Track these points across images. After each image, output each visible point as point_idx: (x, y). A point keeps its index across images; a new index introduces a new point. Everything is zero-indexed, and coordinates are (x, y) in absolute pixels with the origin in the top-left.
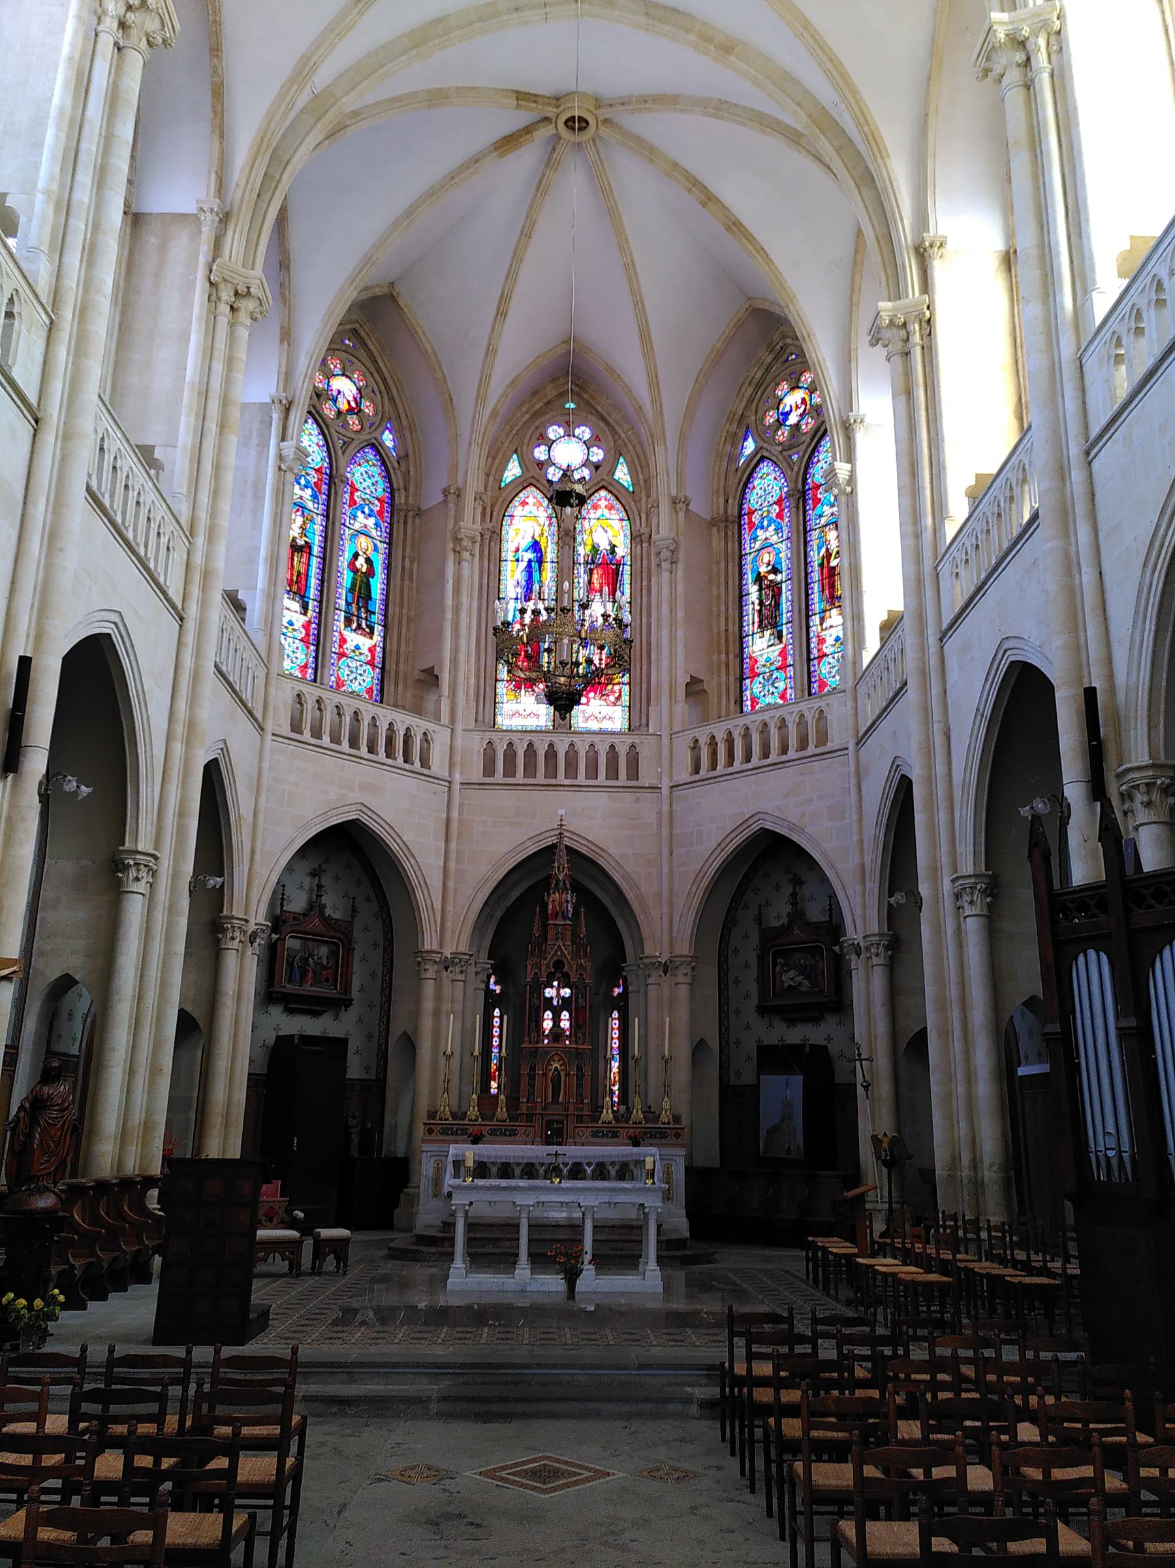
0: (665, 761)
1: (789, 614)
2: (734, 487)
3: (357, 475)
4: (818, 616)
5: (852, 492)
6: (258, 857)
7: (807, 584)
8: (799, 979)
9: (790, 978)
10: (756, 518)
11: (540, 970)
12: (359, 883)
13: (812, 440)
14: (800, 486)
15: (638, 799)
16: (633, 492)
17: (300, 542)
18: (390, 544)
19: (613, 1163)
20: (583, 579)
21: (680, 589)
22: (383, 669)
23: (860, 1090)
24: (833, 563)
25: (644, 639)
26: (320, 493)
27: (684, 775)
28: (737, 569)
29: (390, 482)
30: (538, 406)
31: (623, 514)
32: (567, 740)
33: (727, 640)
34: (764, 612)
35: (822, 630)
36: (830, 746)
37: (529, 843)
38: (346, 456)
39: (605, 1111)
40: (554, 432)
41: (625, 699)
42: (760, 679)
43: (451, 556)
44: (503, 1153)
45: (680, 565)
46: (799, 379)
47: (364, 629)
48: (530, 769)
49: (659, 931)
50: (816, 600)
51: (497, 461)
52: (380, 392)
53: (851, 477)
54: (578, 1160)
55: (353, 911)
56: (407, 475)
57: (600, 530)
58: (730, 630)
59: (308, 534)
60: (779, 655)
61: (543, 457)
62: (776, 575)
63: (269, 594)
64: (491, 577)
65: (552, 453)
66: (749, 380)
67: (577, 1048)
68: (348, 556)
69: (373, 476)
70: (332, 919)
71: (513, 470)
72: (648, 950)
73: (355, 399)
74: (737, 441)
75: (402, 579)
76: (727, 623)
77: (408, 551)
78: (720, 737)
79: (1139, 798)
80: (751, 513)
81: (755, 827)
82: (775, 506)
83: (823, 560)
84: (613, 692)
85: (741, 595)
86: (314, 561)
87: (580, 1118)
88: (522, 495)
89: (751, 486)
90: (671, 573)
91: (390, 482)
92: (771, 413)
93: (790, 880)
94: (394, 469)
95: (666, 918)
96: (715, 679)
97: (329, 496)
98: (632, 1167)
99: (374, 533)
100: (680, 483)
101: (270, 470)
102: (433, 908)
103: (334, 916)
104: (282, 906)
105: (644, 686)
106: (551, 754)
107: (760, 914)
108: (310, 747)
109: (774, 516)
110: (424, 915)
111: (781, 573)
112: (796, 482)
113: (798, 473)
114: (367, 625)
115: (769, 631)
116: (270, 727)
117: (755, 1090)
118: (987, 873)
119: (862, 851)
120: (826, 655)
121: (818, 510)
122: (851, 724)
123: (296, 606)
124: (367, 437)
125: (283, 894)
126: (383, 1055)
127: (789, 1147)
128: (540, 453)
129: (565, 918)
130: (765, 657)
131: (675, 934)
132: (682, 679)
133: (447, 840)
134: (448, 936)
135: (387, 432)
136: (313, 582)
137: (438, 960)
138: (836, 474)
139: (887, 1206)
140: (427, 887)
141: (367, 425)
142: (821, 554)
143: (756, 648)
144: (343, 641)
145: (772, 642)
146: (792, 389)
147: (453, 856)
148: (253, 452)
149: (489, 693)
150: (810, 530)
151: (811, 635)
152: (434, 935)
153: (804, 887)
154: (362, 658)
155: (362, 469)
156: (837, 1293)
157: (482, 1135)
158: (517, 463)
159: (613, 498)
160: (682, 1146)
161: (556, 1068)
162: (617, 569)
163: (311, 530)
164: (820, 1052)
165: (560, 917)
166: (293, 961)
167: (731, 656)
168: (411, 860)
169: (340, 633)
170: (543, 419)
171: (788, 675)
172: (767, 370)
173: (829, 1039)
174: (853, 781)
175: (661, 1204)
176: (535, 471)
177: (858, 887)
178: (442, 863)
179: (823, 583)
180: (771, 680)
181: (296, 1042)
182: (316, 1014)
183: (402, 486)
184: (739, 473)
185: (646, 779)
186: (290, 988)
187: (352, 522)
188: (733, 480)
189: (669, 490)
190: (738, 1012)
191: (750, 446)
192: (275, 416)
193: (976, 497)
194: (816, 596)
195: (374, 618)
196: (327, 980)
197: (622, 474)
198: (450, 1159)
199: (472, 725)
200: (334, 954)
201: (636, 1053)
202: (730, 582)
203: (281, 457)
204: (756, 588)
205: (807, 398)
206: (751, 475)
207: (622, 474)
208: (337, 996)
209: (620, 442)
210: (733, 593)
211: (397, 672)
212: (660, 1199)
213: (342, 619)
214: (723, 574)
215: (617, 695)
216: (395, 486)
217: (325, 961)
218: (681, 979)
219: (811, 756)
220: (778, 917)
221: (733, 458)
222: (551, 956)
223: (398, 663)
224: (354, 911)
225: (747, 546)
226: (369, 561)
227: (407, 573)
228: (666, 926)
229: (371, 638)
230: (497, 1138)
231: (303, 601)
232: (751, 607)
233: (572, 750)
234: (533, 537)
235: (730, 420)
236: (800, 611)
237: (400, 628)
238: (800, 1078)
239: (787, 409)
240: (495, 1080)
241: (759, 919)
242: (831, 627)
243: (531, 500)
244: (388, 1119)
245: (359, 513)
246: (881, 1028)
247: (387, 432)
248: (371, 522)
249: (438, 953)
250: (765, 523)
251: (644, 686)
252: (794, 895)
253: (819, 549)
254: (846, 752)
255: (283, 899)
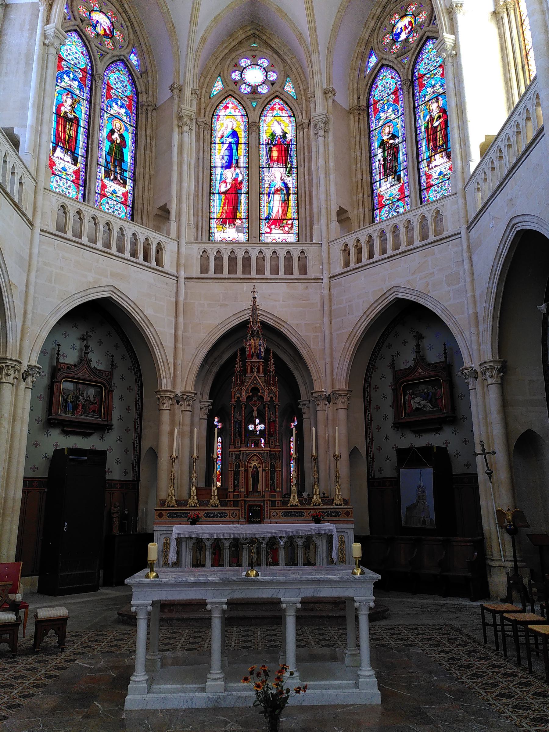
0: (325, 261)
1: (405, 163)
2: (364, 87)
3: (112, 78)
4: (425, 161)
5: (456, 55)
6: (29, 317)
7: (417, 142)
8: (424, 402)
9: (416, 402)
10: (379, 106)
11: (241, 395)
12: (116, 346)
13: (418, 45)
14: (410, 78)
15: (307, 287)
16: (297, 99)
17: (71, 116)
18: (136, 128)
19: (300, 537)
20: (264, 153)
21: (331, 148)
22: (133, 208)
23: (482, 477)
24: (436, 124)
25: (307, 189)
26: (85, 85)
27: (338, 269)
28: (367, 140)
29: (136, 87)
30: (233, 44)
31: (290, 113)
32: (258, 248)
33: (362, 186)
34: (388, 165)
35: (429, 169)
36: (445, 234)
37: (233, 318)
38: (103, 63)
39: (292, 497)
40: (244, 62)
41: (295, 229)
42: (386, 208)
43: (176, 130)
44: (215, 532)
45: (331, 133)
46: (406, 10)
47: (119, 180)
48: (232, 269)
49: (324, 375)
50: (424, 150)
51: (207, 79)
52: (127, 27)
53: (455, 44)
54: (273, 535)
55: (112, 365)
56: (147, 84)
57: (276, 123)
58: (364, 179)
59: (76, 111)
60: (399, 191)
61: (238, 78)
62: (394, 140)
63: (37, 131)
64: (206, 153)
65: (243, 76)
66: (372, 16)
67: (270, 451)
68: (106, 131)
69: (124, 82)
70: (96, 369)
71: (218, 87)
72: (316, 388)
73: (109, 29)
74: (364, 57)
75: (145, 150)
76: (362, 175)
77: (149, 131)
78: (363, 240)
79: (488, 374)
80: (376, 103)
81: (391, 298)
82: (392, 96)
83: (428, 124)
84: (287, 225)
85: (371, 157)
86: (81, 131)
87: (273, 503)
88: (225, 103)
89: (375, 86)
90: (325, 138)
91: (136, 87)
92: (387, 36)
93: (414, 336)
94: (138, 78)
95: (328, 365)
96: (356, 211)
97: (91, 89)
98: (315, 539)
99: (125, 119)
100: (329, 81)
101: (37, 47)
102: (167, 362)
103: (98, 368)
104: (58, 359)
105: (308, 219)
106: (247, 260)
107: (393, 361)
108: (72, 243)
109: (391, 102)
110: (161, 366)
111: (398, 138)
112: (407, 75)
113: (408, 69)
114: (121, 178)
115: (391, 177)
116: (38, 224)
117: (395, 482)
118: (501, 359)
119: (475, 303)
120: (433, 186)
121: (423, 92)
122: (462, 214)
123: (68, 158)
124: (119, 53)
125: (59, 351)
126: (137, 464)
127: (424, 520)
128: (236, 76)
129: (258, 357)
130: (389, 193)
131: (335, 376)
132: (335, 209)
133: (176, 316)
134: (178, 380)
135: (133, 55)
136: (81, 144)
137: (172, 396)
138: (444, 43)
139: (512, 564)
140: (163, 347)
141: (118, 46)
142: (427, 120)
143: (383, 188)
144: (104, 186)
145: (394, 183)
146: (402, 17)
147: (181, 326)
148: (26, 34)
149: (206, 227)
150: (419, 106)
151: (421, 174)
152: (169, 380)
153: (424, 341)
154: (118, 199)
155: (116, 76)
156: (530, 664)
157: (198, 517)
158: (220, 82)
159: (283, 103)
160: (351, 522)
161: (255, 466)
162: (288, 147)
163: (79, 109)
164: (443, 451)
165: (255, 356)
166: (67, 398)
167: (366, 196)
168: (150, 328)
169: (102, 180)
170: (237, 53)
171: (406, 203)
172: (385, 8)
173: (447, 443)
174: (466, 255)
175: (374, 598)
176: (232, 86)
177: (473, 330)
178: (173, 331)
179: (428, 139)
180: (393, 206)
181: (66, 453)
182: (87, 435)
183: (144, 90)
184: (367, 78)
185: (312, 273)
186: (64, 416)
187: (109, 109)
188: (363, 83)
189: (322, 84)
190: (378, 428)
191: (373, 60)
192: (41, 9)
193: (485, 150)
194: (424, 149)
195: (126, 174)
196: (94, 411)
197: (289, 88)
198: (174, 537)
199: (193, 240)
200: (99, 394)
201: (314, 454)
202: (363, 148)
203: (45, 36)
204: (380, 151)
205: (413, 21)
206: (375, 79)
207: (289, 88)
208: (100, 423)
209: (287, 67)
210: (365, 156)
211: (142, 210)
212: (371, 591)
213: (103, 172)
214: (358, 143)
215: (290, 226)
216: (139, 90)
217: (92, 399)
218: (340, 406)
219: (431, 243)
220: (406, 363)
221: (362, 70)
222: (249, 384)
223: (143, 204)
224: (113, 365)
225: (374, 125)
226: (121, 136)
227: (148, 146)
228: (328, 371)
229: (125, 187)
230: (211, 520)
231: (74, 156)
232: (377, 163)
233: (261, 258)
234: (232, 128)
235: (360, 44)
236: (413, 159)
237: (144, 181)
238: (431, 470)
239: (399, 30)
240: (219, 481)
241: (392, 365)
242: (435, 166)
243: (230, 105)
244: (141, 506)
245: (114, 104)
246: (497, 430)
247: (133, 55)
248: (123, 111)
249: (172, 392)
250: (386, 108)
251: (308, 219)
252: (418, 346)
253: (425, 117)
254: (459, 236)
255: (58, 354)
